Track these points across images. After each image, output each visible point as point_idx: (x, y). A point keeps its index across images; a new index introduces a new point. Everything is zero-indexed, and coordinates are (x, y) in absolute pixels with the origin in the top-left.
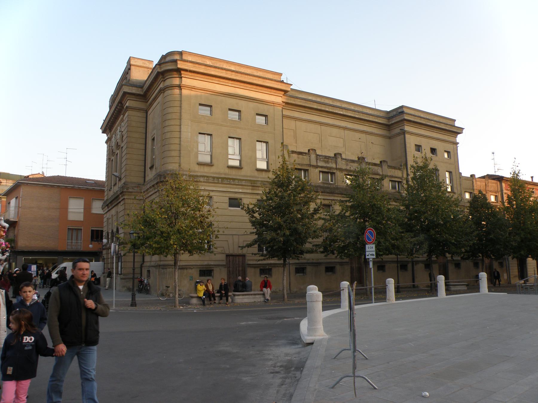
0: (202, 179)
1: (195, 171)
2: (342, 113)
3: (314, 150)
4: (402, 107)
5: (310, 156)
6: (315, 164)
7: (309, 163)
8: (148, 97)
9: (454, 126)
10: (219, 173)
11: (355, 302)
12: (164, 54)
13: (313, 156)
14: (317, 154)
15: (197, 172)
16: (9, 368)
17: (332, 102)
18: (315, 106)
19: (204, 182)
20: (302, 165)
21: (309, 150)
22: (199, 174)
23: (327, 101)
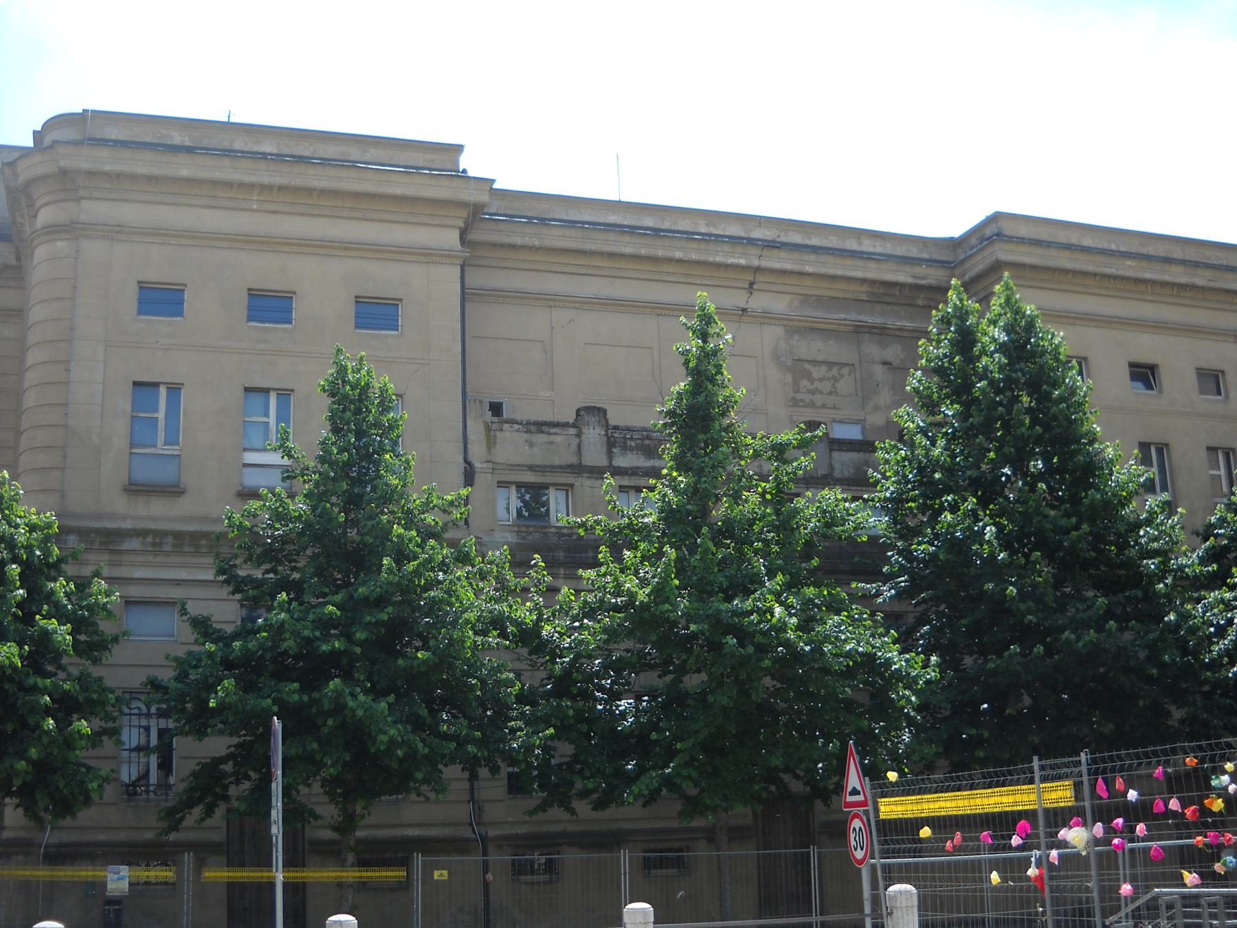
0: (135, 544)
1: (113, 516)
2: (743, 262)
3: (600, 409)
4: (996, 218)
5: (579, 435)
6: (602, 461)
7: (573, 460)
8: (850, 325)
9: (463, 176)
10: (205, 519)
11: (809, 852)
12: (471, 164)
13: (593, 435)
14: (612, 422)
15: (124, 518)
16: (445, 872)
17: (707, 225)
18: (627, 246)
19: (143, 552)
20: (551, 469)
21: (578, 414)
22: (128, 525)
23: (867, 246)
